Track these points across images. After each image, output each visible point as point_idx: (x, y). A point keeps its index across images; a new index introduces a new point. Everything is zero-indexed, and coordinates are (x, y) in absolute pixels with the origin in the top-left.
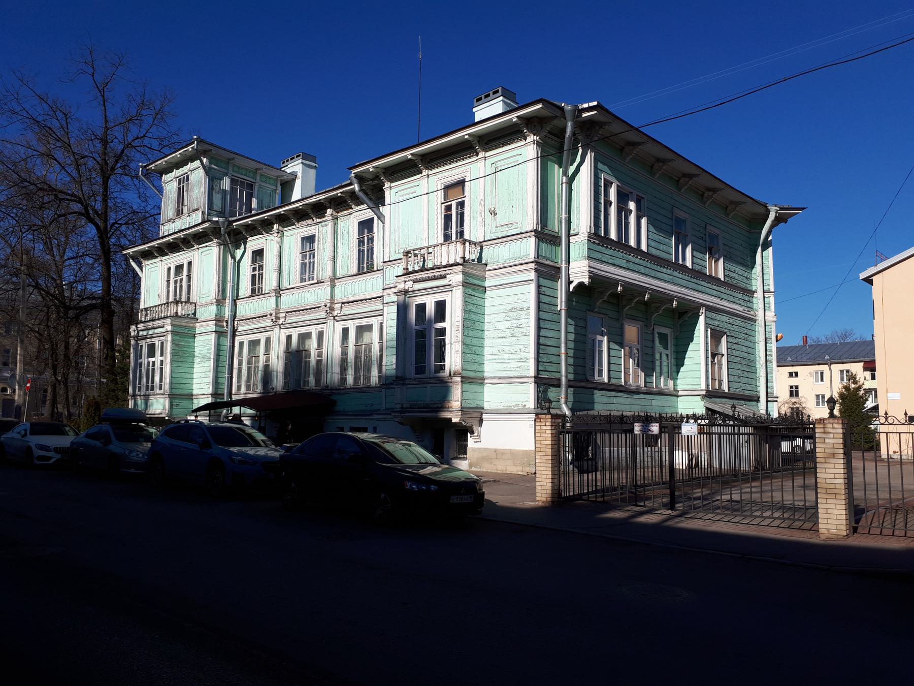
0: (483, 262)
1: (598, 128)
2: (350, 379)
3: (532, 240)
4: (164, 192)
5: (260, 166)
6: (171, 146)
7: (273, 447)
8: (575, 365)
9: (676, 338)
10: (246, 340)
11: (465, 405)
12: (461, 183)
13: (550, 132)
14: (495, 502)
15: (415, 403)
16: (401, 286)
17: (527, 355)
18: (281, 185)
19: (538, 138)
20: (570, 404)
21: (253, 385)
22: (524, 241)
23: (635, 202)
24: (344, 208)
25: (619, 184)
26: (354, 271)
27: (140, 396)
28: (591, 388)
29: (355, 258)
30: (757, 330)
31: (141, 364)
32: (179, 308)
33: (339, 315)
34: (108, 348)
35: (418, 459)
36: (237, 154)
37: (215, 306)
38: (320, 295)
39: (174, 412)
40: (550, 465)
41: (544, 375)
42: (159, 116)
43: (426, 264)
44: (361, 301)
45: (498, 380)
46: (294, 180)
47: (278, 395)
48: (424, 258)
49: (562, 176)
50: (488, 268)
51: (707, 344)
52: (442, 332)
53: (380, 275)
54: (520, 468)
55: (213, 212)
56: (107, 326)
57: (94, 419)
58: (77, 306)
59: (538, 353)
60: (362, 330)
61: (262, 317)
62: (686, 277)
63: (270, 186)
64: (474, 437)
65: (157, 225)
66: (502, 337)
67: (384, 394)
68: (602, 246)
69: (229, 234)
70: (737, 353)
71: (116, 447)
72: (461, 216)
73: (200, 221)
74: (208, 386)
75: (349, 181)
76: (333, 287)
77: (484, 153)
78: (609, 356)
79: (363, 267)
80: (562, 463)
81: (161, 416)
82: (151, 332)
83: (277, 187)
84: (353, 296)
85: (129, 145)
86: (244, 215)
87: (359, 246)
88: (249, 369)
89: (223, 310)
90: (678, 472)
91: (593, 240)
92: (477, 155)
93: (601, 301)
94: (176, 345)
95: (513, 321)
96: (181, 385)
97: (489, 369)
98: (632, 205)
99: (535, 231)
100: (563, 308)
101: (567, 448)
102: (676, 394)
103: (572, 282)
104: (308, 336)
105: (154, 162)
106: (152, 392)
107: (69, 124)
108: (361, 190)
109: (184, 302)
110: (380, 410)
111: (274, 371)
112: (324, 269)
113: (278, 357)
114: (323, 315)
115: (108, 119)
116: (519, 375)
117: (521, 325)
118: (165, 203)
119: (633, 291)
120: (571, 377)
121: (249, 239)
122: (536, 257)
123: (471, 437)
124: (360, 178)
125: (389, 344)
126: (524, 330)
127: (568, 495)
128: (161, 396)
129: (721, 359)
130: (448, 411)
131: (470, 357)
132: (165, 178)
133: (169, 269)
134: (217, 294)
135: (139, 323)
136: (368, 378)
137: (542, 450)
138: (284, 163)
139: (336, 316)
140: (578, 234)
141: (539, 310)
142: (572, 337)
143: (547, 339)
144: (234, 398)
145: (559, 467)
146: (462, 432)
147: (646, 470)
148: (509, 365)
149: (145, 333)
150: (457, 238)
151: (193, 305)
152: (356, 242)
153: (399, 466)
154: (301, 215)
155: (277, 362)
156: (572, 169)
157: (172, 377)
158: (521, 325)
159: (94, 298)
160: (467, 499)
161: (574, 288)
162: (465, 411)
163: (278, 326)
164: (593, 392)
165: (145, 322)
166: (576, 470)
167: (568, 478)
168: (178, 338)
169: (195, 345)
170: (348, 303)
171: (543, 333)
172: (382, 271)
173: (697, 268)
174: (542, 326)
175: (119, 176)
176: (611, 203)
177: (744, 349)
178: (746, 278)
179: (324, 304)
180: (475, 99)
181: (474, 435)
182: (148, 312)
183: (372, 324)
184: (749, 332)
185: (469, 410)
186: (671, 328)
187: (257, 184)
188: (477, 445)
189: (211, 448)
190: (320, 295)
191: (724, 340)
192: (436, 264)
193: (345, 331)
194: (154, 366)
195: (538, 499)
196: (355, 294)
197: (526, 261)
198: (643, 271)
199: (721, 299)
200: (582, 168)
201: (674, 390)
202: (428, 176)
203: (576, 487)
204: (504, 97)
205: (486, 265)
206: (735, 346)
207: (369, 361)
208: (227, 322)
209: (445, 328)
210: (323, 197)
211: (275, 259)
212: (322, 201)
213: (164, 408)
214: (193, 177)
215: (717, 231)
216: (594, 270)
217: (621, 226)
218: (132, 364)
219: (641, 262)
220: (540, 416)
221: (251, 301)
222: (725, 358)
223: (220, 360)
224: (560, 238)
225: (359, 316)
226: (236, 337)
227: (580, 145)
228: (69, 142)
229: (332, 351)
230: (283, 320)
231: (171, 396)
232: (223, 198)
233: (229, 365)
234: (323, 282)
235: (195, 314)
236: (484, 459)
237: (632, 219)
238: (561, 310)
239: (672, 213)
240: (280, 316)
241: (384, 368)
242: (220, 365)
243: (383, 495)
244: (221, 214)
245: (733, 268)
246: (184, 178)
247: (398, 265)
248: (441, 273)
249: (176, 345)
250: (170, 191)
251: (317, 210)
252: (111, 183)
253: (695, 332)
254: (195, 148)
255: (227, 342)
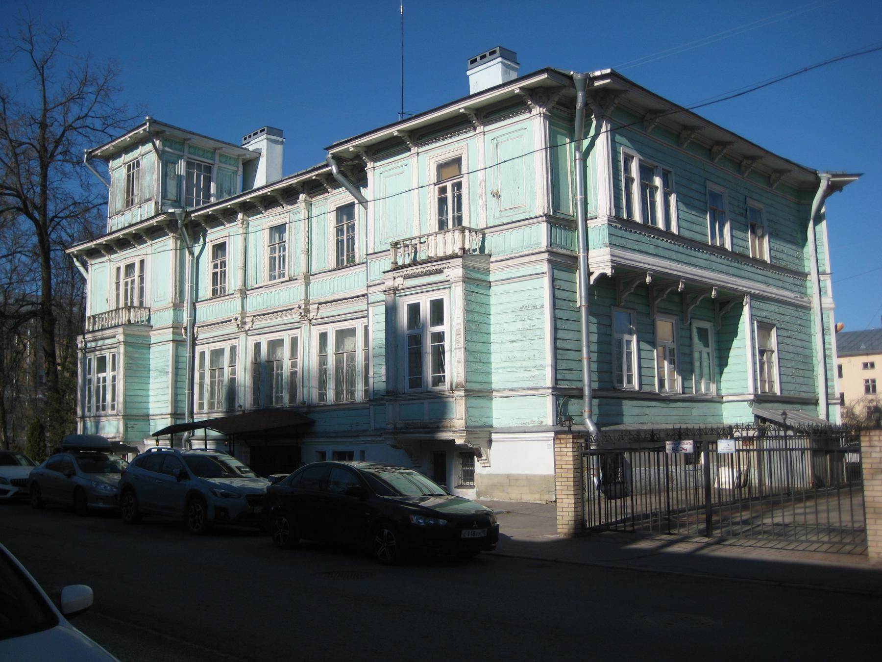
0: (487, 252)
1: (613, 97)
2: (331, 394)
3: (544, 226)
4: (112, 180)
5: (218, 145)
6: (115, 125)
7: (252, 475)
8: (600, 371)
9: (718, 333)
10: (207, 349)
11: (471, 424)
12: (458, 161)
13: (558, 103)
14: (509, 535)
15: (410, 422)
16: (390, 284)
17: (542, 362)
18: (243, 164)
19: (545, 110)
20: (595, 418)
21: (218, 403)
22: (534, 227)
23: (660, 177)
24: (319, 192)
25: (642, 158)
26: (332, 264)
27: (90, 417)
28: (619, 398)
29: (333, 249)
30: (812, 319)
31: (90, 381)
32: (132, 314)
33: (315, 317)
34: (49, 362)
35: (421, 490)
36: (193, 134)
37: (172, 311)
38: (293, 294)
39: (129, 436)
40: (572, 492)
41: (564, 385)
42: (103, 93)
43: (418, 256)
44: (341, 300)
45: (509, 392)
46: (258, 159)
47: (245, 415)
48: (416, 249)
49: (575, 152)
50: (492, 259)
51: (753, 339)
52: (440, 337)
53: (363, 269)
54: (537, 496)
55: (166, 201)
56: (48, 336)
57: (39, 445)
58: (15, 314)
59: (555, 360)
60: (343, 335)
61: (226, 322)
62: (725, 262)
63: (231, 167)
64: (482, 462)
65: (102, 218)
66: (512, 341)
67: (372, 412)
68: (626, 230)
69: (186, 226)
70: (790, 348)
71: (81, 479)
72: (458, 199)
73: (153, 215)
74: (166, 405)
75: (325, 163)
76: (307, 284)
77: (482, 127)
78: (639, 358)
79: (343, 261)
80: (587, 489)
81: (114, 440)
82: (100, 343)
83: (238, 167)
84: (332, 295)
85: (70, 128)
86: (201, 206)
87: (337, 235)
88: (212, 384)
89: (181, 314)
90: (724, 493)
91: (614, 225)
92: (475, 129)
93: (627, 294)
94: (130, 357)
95: (525, 322)
96: (136, 404)
97: (498, 380)
98: (658, 181)
99: (547, 215)
100: (583, 303)
101: (592, 471)
102: (718, 399)
103: (593, 273)
104: (279, 343)
105: (100, 148)
106: (102, 413)
107: (6, 110)
108: (340, 172)
109: (136, 307)
110: (367, 430)
111: (240, 386)
112: (296, 264)
113: (245, 369)
114: (296, 318)
115: (48, 100)
116: (534, 385)
117: (534, 326)
118: (112, 192)
119: (664, 281)
120: (595, 385)
121: (209, 232)
122: (549, 246)
123: (478, 461)
124: (338, 159)
125: (377, 351)
126: (538, 332)
127: (593, 525)
128: (114, 417)
129: (771, 356)
130: (450, 431)
131: (474, 366)
132: (113, 164)
133: (118, 269)
134: (174, 296)
135: (87, 333)
136: (352, 393)
137: (563, 475)
138: (245, 139)
139: (312, 319)
140: (596, 218)
141: (554, 307)
142: (594, 338)
143: (565, 342)
144: (197, 419)
145: (583, 494)
146: (468, 455)
147: (679, 492)
148: (522, 375)
149: (93, 344)
150: (454, 225)
151: (147, 310)
152: (333, 231)
153: (398, 498)
154: (268, 202)
155: (244, 377)
156: (586, 143)
157: (125, 395)
158: (534, 326)
159: (33, 304)
160: (480, 533)
161: (595, 280)
162: (471, 431)
163: (245, 332)
164: (621, 403)
165: (93, 331)
166: (602, 495)
167: (593, 505)
168: (131, 349)
169: (151, 357)
170: (326, 303)
171: (561, 334)
172: (365, 265)
173: (738, 250)
174: (558, 327)
175: (59, 163)
176: (633, 180)
177: (798, 343)
178: (797, 258)
179: (297, 306)
180: (469, 61)
181: (482, 458)
182: (97, 319)
183: (355, 328)
184: (803, 323)
185: (475, 430)
186: (710, 321)
187: (216, 167)
188: (486, 471)
189: (189, 479)
190: (293, 294)
191: (773, 333)
192: (430, 255)
193: (323, 337)
194: (105, 382)
195: (559, 531)
196: (334, 293)
197: (537, 251)
198: (674, 257)
199: (768, 285)
200: (597, 142)
201: (718, 394)
202: (418, 154)
203: (603, 515)
204: (503, 57)
205: (490, 256)
206: (787, 341)
207: (352, 373)
208: (186, 329)
209: (443, 332)
210: (295, 181)
211: (240, 254)
212: (294, 186)
213: (118, 431)
214: (144, 163)
215: (761, 206)
216: (617, 259)
217: (646, 206)
218: (80, 380)
219: (672, 246)
220: (559, 436)
221: (212, 304)
222: (775, 354)
223: (179, 374)
224: (576, 222)
225: (339, 318)
226: (196, 347)
227: (593, 116)
228: (7, 129)
229: (309, 361)
230: (250, 325)
231: (125, 417)
232: (178, 184)
233: (189, 379)
234: (296, 279)
235: (149, 320)
236: (494, 486)
237: (659, 197)
238: (580, 306)
239: (705, 187)
240: (247, 321)
241: (371, 381)
242: (179, 380)
243: (386, 531)
244: (176, 203)
245: (780, 248)
246: (134, 164)
247: (384, 257)
248: (437, 267)
249: (130, 357)
250: (119, 180)
251: (289, 195)
252: (51, 172)
253: (739, 326)
254: (148, 130)
255: (187, 353)
